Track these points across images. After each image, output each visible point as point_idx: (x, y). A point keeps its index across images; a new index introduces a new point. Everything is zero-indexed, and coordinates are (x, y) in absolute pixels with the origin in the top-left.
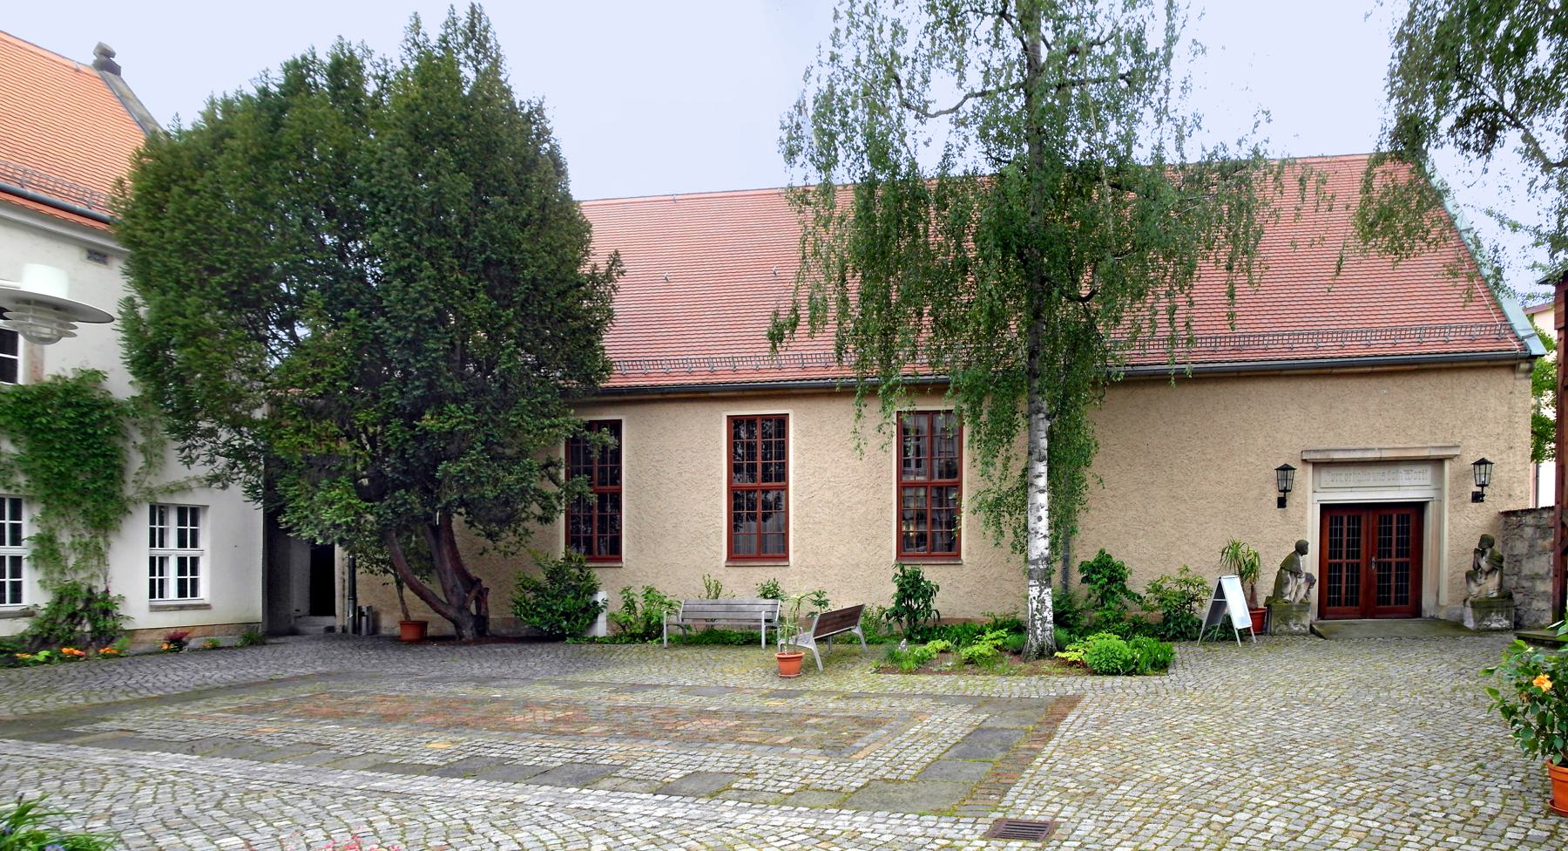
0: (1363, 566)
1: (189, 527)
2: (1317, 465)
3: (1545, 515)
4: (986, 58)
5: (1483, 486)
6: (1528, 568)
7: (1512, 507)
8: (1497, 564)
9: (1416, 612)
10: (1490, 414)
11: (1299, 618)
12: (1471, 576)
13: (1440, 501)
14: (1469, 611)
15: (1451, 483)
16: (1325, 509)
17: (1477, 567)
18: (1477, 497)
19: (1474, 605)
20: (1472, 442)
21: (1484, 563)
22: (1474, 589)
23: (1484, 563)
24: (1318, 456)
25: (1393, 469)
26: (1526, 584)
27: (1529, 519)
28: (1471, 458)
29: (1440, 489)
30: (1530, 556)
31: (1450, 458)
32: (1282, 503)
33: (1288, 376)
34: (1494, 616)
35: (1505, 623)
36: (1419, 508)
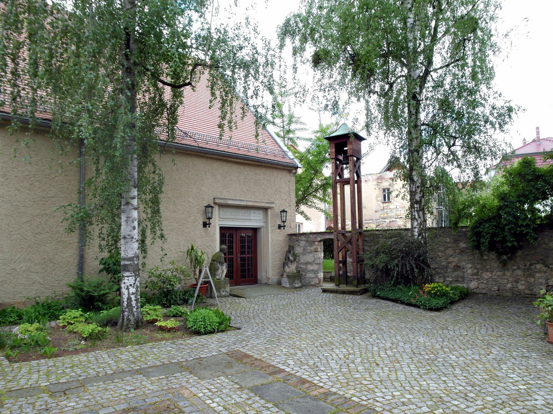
0: (235, 260)
2: (221, 206)
3: (311, 236)
4: (431, 89)
10: (283, 190)
13: (267, 227)
16: (222, 228)
19: (288, 277)
24: (222, 201)
27: (303, 238)
28: (278, 209)
29: (266, 222)
30: (304, 254)
31: (270, 208)
32: (205, 225)
33: (207, 158)
34: (297, 281)
36: (255, 230)
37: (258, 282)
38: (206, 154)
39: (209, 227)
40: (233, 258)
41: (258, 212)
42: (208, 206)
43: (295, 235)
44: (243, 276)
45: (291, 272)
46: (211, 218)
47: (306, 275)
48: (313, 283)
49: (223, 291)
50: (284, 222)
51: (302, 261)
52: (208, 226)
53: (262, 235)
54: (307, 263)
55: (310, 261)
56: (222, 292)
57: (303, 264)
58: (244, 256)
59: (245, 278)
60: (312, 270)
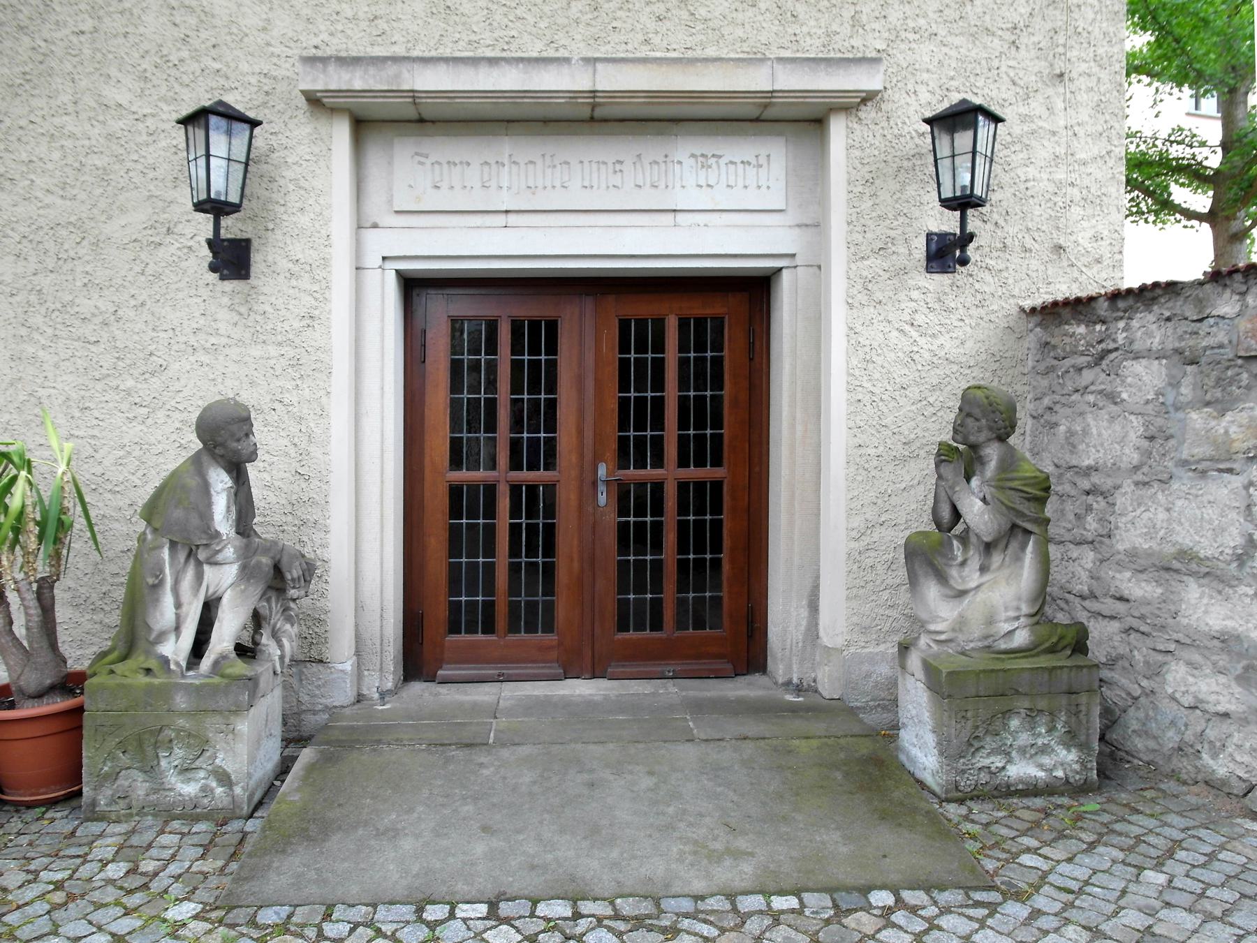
0: (567, 498)
1: (483, 357)
2: (371, 123)
5: (963, 203)
6: (1143, 522)
7: (1064, 290)
8: (1028, 512)
9: (748, 652)
11: (201, 745)
12: (927, 556)
14: (916, 701)
15: (854, 199)
17: (950, 519)
18: (946, 254)
20: (925, 53)
21: (977, 512)
22: (941, 611)
23: (977, 512)
25: (651, 148)
26: (1141, 589)
27: (1147, 329)
29: (816, 226)
30: (1149, 477)
32: (232, 259)
35: (1064, 760)
36: (752, 291)
40: (551, 488)
43: (1078, 307)
45: (973, 636)
47: (1156, 672)
48: (1220, 768)
49: (185, 771)
51: (1130, 537)
54: (1178, 565)
55: (1206, 549)
56: (172, 779)
57: (1139, 563)
58: (650, 473)
59: (657, 625)
60: (1226, 641)
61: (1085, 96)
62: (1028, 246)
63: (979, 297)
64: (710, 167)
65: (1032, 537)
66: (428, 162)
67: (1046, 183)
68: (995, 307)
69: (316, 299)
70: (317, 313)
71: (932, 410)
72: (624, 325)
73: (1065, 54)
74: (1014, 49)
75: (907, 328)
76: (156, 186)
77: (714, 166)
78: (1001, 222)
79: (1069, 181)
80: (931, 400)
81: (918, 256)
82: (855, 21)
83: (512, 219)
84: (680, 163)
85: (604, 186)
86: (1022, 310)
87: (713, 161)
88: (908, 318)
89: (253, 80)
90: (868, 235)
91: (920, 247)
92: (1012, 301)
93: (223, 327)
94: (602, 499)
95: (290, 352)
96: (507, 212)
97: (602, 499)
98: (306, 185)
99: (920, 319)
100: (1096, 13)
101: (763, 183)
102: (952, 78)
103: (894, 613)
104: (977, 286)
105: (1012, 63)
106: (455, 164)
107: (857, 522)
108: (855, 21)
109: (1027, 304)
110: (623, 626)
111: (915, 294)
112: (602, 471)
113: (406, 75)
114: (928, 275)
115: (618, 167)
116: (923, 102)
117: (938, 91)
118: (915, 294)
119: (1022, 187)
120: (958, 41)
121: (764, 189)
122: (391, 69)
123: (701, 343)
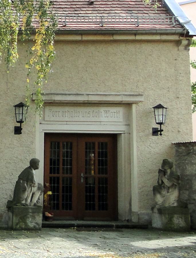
0: (75, 180)
10: (163, 74)
12: (158, 188)
16: (47, 136)
25: (95, 109)
29: (129, 125)
31: (136, 103)
36: (114, 138)
37: (120, 218)
38: (135, 34)
39: (161, 134)
40: (71, 179)
41: (113, 110)
42: (21, 105)
44: (90, 207)
46: (23, 122)
50: (161, 124)
52: (159, 133)
53: (122, 143)
61: (183, 101)
62: (173, 131)
63: (163, 141)
64: (107, 113)
65: (177, 186)
66: (52, 111)
67: (176, 118)
68: (166, 143)
69: (33, 138)
70: (33, 141)
71: (155, 163)
72: (86, 144)
73: (179, 93)
74: (168, 92)
75: (149, 147)
76: (3, 116)
77: (108, 113)
78: (167, 126)
79: (181, 118)
80: (154, 161)
81: (151, 132)
82: (137, 86)
83: (68, 123)
84: (101, 112)
85: (86, 116)
86: (172, 143)
87: (108, 112)
88: (149, 145)
89: (21, 96)
90: (141, 128)
91: (151, 131)
92: (170, 142)
93: (15, 144)
94: (82, 181)
95: (28, 149)
96: (67, 121)
97: (82, 181)
98: (31, 116)
99: (152, 145)
100: (185, 85)
101: (118, 116)
102: (156, 97)
103: (148, 205)
104: (163, 138)
105: (168, 94)
106: (57, 112)
107: (140, 186)
108: (137, 86)
109: (173, 142)
110: (86, 209)
111: (150, 140)
112: (82, 175)
113: (53, 97)
114: (153, 136)
115: (89, 113)
116: (151, 102)
117: (154, 100)
118: (150, 140)
119: (171, 119)
120: (157, 90)
121: (118, 118)
122: (50, 96)
123: (106, 148)
